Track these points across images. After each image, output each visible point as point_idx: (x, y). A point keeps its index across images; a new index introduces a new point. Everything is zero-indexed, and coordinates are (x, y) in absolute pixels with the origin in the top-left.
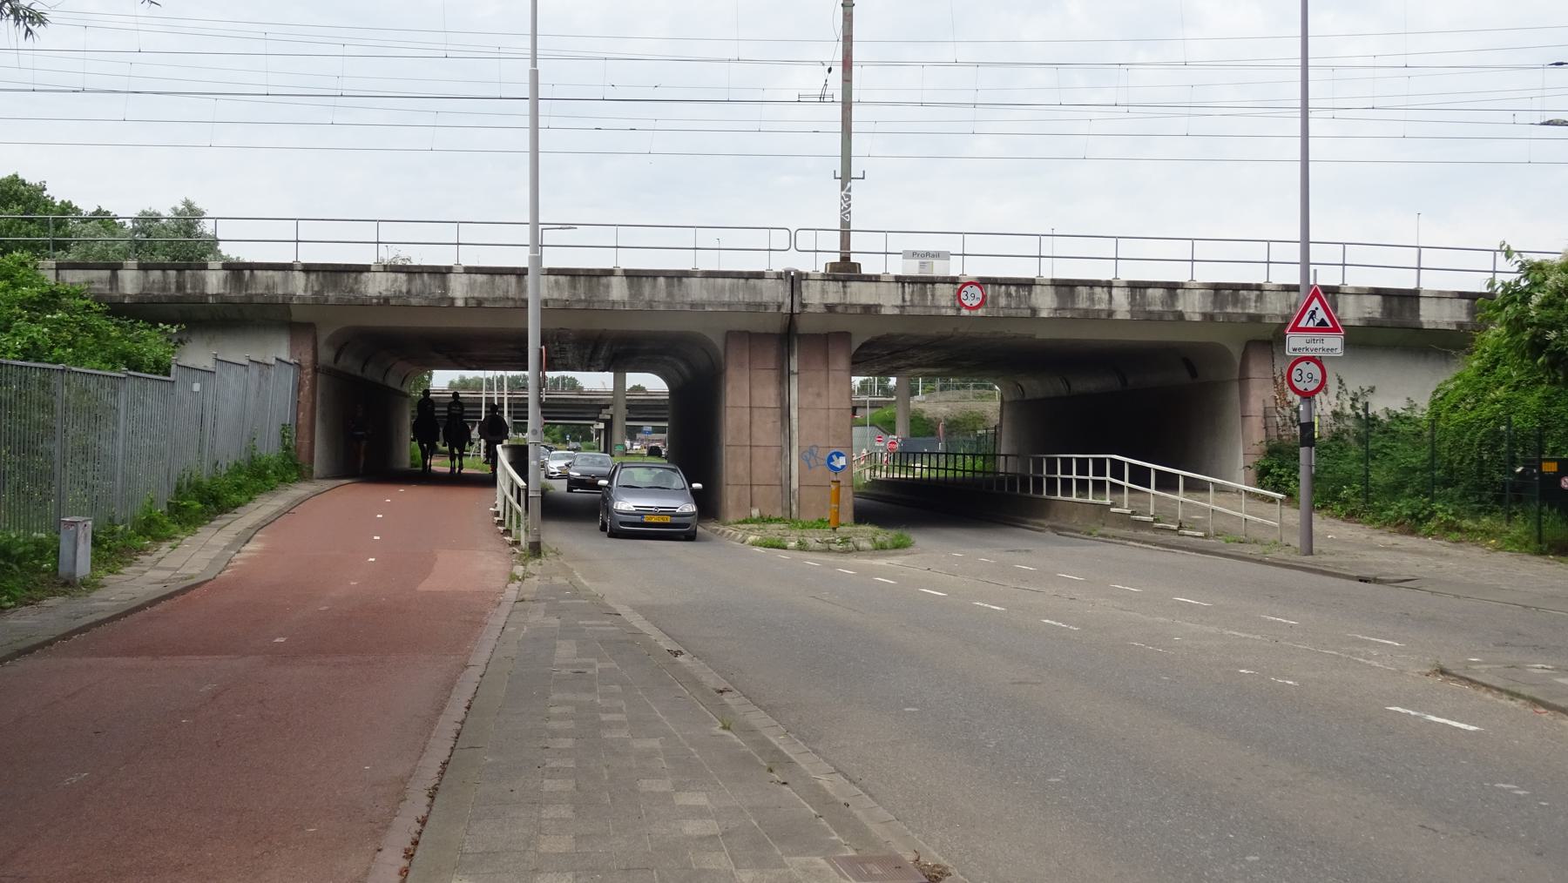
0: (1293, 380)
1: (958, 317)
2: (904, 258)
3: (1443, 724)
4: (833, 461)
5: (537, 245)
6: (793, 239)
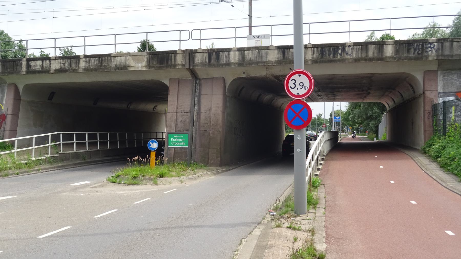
0: (290, 88)
1: (43, 58)
2: (248, 39)
3: (146, 200)
4: (151, 145)
5: (298, 33)
6: (191, 35)
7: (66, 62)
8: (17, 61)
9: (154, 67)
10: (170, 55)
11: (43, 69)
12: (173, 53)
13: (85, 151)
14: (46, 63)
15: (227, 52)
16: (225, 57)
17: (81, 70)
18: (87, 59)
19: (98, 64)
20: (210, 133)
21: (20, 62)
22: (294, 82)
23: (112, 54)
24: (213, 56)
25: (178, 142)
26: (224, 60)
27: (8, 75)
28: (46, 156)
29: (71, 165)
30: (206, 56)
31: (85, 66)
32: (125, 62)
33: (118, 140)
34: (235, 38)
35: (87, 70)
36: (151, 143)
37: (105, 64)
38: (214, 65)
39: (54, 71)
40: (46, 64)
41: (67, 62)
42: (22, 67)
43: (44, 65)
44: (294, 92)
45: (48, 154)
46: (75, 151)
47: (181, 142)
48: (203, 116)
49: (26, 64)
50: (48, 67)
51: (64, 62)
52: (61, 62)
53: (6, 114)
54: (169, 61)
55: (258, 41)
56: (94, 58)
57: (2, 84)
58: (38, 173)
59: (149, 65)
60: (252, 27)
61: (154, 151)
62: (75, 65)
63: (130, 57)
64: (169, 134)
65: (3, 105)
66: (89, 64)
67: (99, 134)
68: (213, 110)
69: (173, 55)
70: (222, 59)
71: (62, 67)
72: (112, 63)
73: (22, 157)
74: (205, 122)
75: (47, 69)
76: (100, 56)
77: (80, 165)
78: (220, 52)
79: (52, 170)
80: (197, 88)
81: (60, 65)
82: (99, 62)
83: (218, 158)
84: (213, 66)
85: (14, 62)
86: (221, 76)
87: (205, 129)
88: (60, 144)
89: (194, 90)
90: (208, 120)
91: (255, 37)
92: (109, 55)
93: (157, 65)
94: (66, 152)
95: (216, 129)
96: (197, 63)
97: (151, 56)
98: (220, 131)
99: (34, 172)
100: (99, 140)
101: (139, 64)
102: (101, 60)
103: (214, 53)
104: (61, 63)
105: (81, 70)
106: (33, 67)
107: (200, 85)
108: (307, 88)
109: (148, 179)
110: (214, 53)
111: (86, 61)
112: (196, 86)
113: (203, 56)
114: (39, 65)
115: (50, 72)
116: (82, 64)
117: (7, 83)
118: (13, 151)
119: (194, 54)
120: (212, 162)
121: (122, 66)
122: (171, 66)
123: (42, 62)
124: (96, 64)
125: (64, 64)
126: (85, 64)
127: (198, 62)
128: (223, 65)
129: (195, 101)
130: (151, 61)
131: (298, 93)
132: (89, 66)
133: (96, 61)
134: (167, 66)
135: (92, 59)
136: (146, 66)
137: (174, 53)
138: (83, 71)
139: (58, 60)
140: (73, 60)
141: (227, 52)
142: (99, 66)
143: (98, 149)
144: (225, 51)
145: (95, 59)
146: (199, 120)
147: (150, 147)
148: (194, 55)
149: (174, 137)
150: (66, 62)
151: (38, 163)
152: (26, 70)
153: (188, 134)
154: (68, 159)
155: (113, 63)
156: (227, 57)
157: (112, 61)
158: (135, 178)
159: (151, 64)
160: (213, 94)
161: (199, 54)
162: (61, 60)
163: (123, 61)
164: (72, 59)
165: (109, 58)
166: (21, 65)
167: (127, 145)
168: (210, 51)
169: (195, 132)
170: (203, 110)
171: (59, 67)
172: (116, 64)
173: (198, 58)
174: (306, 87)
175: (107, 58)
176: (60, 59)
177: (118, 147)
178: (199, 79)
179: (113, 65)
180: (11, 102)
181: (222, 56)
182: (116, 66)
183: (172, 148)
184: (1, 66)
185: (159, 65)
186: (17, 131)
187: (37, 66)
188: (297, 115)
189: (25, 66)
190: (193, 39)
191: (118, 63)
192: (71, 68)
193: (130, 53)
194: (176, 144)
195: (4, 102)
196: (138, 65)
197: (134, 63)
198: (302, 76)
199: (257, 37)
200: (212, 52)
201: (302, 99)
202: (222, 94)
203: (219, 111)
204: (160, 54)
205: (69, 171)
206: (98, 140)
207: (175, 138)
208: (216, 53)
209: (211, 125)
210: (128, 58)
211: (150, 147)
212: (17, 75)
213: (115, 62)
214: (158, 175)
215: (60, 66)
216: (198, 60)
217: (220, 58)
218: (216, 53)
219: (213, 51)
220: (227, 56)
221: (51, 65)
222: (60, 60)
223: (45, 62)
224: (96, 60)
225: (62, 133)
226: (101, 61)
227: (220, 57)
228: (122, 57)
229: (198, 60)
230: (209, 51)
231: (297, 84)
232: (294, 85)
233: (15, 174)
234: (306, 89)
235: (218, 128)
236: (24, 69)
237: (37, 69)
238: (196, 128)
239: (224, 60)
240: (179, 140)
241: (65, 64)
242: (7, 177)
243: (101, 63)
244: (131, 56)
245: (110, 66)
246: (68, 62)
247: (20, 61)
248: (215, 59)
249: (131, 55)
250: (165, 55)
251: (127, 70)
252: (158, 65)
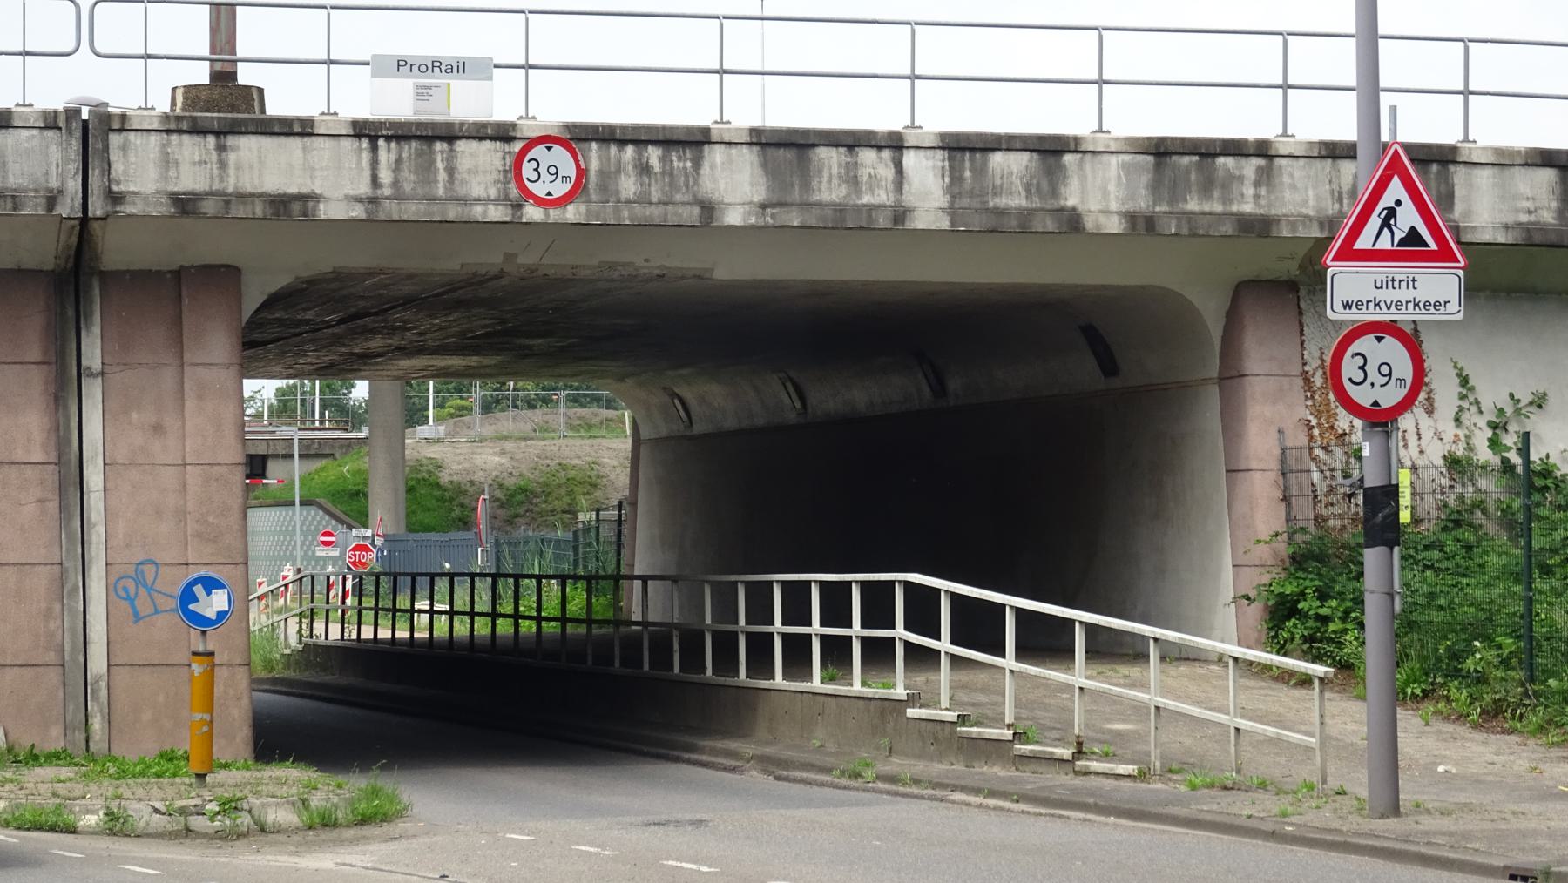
2: (374, 75)
22: (534, 164)
34: (722, 72)
55: (430, 88)
60: (238, 8)
91: (415, 68)
147: (191, 607)
190: (100, 48)
198: (1389, 340)
199: (423, 68)
211: (191, 607)
231: (1371, 369)
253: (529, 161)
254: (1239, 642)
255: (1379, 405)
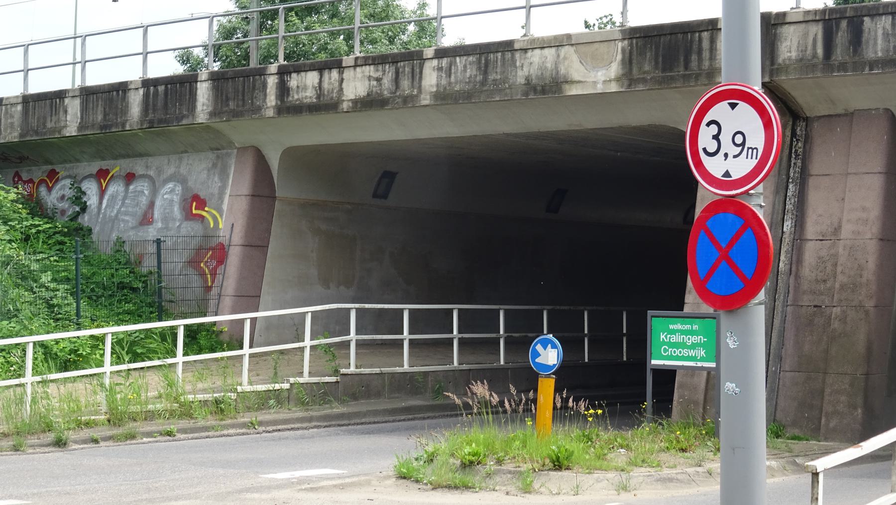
7: (384, 71)
8: (254, 76)
9: (644, 81)
10: (697, 34)
11: (322, 99)
12: (707, 30)
13: (447, 367)
14: (330, 79)
15: (890, 17)
16: (883, 34)
17: (426, 100)
18: (445, 62)
19: (476, 76)
20: (833, 316)
21: (263, 77)
22: (714, 129)
23: (518, 40)
24: (839, 34)
25: (683, 345)
26: (879, 47)
27: (229, 121)
28: (292, 380)
29: (376, 413)
30: (816, 34)
31: (437, 85)
32: (556, 68)
33: (586, 335)
35: (443, 97)
36: (539, 348)
37: (496, 77)
38: (843, 67)
39: (350, 104)
40: (330, 83)
41: (389, 72)
42: (265, 95)
43: (326, 85)
44: (715, 166)
45: (301, 374)
46: (406, 366)
47: (693, 346)
48: (811, 252)
49: (277, 83)
50: (335, 91)
51: (379, 74)
52: (372, 74)
53: (226, 243)
54: (694, 57)
56: (462, 55)
57: (224, 149)
58: (243, 434)
59: (628, 76)
61: (548, 376)
62: (410, 84)
63: (570, 47)
64: (653, 319)
65: (221, 216)
66: (450, 76)
67: (506, 311)
68: (847, 231)
69: (705, 35)
70: (871, 42)
71: (374, 89)
72: (516, 72)
73: (200, 386)
74: (817, 275)
75: (332, 98)
76: (480, 49)
77: (410, 417)
78: (866, 19)
79: (296, 426)
80: (796, 151)
81: (367, 82)
82: (479, 68)
83: (855, 408)
84: (839, 71)
85: (246, 78)
86: (882, 106)
87: (816, 303)
88: (346, 345)
89: (785, 159)
90: (829, 267)
92: (507, 46)
93: (652, 75)
94: (367, 371)
95: (854, 304)
96: (784, 60)
97: (637, 43)
98: (867, 313)
99: (231, 431)
100: (506, 331)
101: (597, 71)
102: (483, 62)
103: (844, 24)
104: (370, 78)
105: (425, 99)
106: (295, 92)
107: (808, 140)
108: (755, 151)
109: (510, 472)
110: (844, 24)
111: (440, 69)
112: (794, 144)
113: (806, 35)
114: (311, 86)
115: (341, 106)
116: (431, 79)
117: (236, 145)
118: (170, 361)
119: (776, 29)
120: (832, 425)
121: (547, 82)
122: (697, 77)
123: (319, 77)
124: (471, 76)
125: (378, 80)
126: (439, 78)
127: (790, 59)
128: (873, 64)
129: (788, 199)
130: (634, 61)
131: (727, 174)
132: (450, 83)
133: (468, 66)
134: (684, 76)
135: (458, 59)
136: (618, 79)
137: (710, 28)
138: (431, 100)
139: (364, 67)
140: (404, 67)
141: (890, 17)
142: (479, 82)
143: (502, 363)
144: (881, 11)
145: (466, 60)
146: (798, 270)
148: (775, 34)
149: (671, 327)
150: (384, 74)
151: (263, 401)
152: (277, 103)
153: (714, 318)
154: (378, 395)
155: (520, 73)
156: (888, 34)
157: (518, 64)
158: (467, 465)
159: (635, 70)
160: (850, 174)
161: (792, 28)
162: (372, 67)
163: (549, 65)
164: (402, 64)
165: (508, 55)
166: (263, 86)
167: (625, 354)
168: (831, 17)
169: (783, 311)
170: (811, 230)
171: (366, 90)
172: (529, 76)
173: (789, 44)
174: (753, 149)
175: (503, 56)
176: (370, 65)
177: (586, 360)
178: (806, 119)
179: (520, 77)
180: (243, 204)
181: (873, 33)
182: (528, 80)
183: (702, 368)
184: (213, 94)
185: (661, 74)
186: (260, 296)
187: (305, 88)
188: (725, 256)
189: (275, 91)
191: (534, 71)
192: (398, 94)
193: (569, 36)
194: (677, 352)
195: (225, 207)
196: (595, 77)
197: (582, 68)
198: (742, 106)
200: (835, 19)
201: (737, 195)
202: (880, 173)
203: (869, 236)
204: (665, 35)
205: (350, 433)
206: (502, 332)
207: (673, 332)
208: (851, 20)
209: (837, 286)
210: (564, 51)
212: (252, 119)
213: (524, 69)
214: (547, 461)
215: (368, 86)
216: (790, 52)
217: (864, 39)
218: (851, 20)
219: (838, 16)
220: (890, 32)
221: (344, 85)
222: (368, 67)
223: (326, 74)
224: (470, 64)
225: (357, 306)
226: (483, 65)
227: (865, 35)
228: (546, 51)
229: (790, 52)
230: (827, 17)
231: (726, 138)
232: (715, 143)
233: (161, 434)
234: (752, 158)
235: (860, 298)
236: (271, 101)
237: (306, 97)
238: (784, 296)
239: (879, 47)
240: (686, 339)
241: (381, 79)
242: (128, 442)
243: (485, 73)
244: (572, 45)
245: (511, 81)
246: (390, 74)
247: (260, 75)
248: (847, 44)
249: (573, 42)
250: (680, 36)
251: (562, 92)
252: (659, 74)
253: (708, 125)
254: (565, 361)
255: (730, 177)
